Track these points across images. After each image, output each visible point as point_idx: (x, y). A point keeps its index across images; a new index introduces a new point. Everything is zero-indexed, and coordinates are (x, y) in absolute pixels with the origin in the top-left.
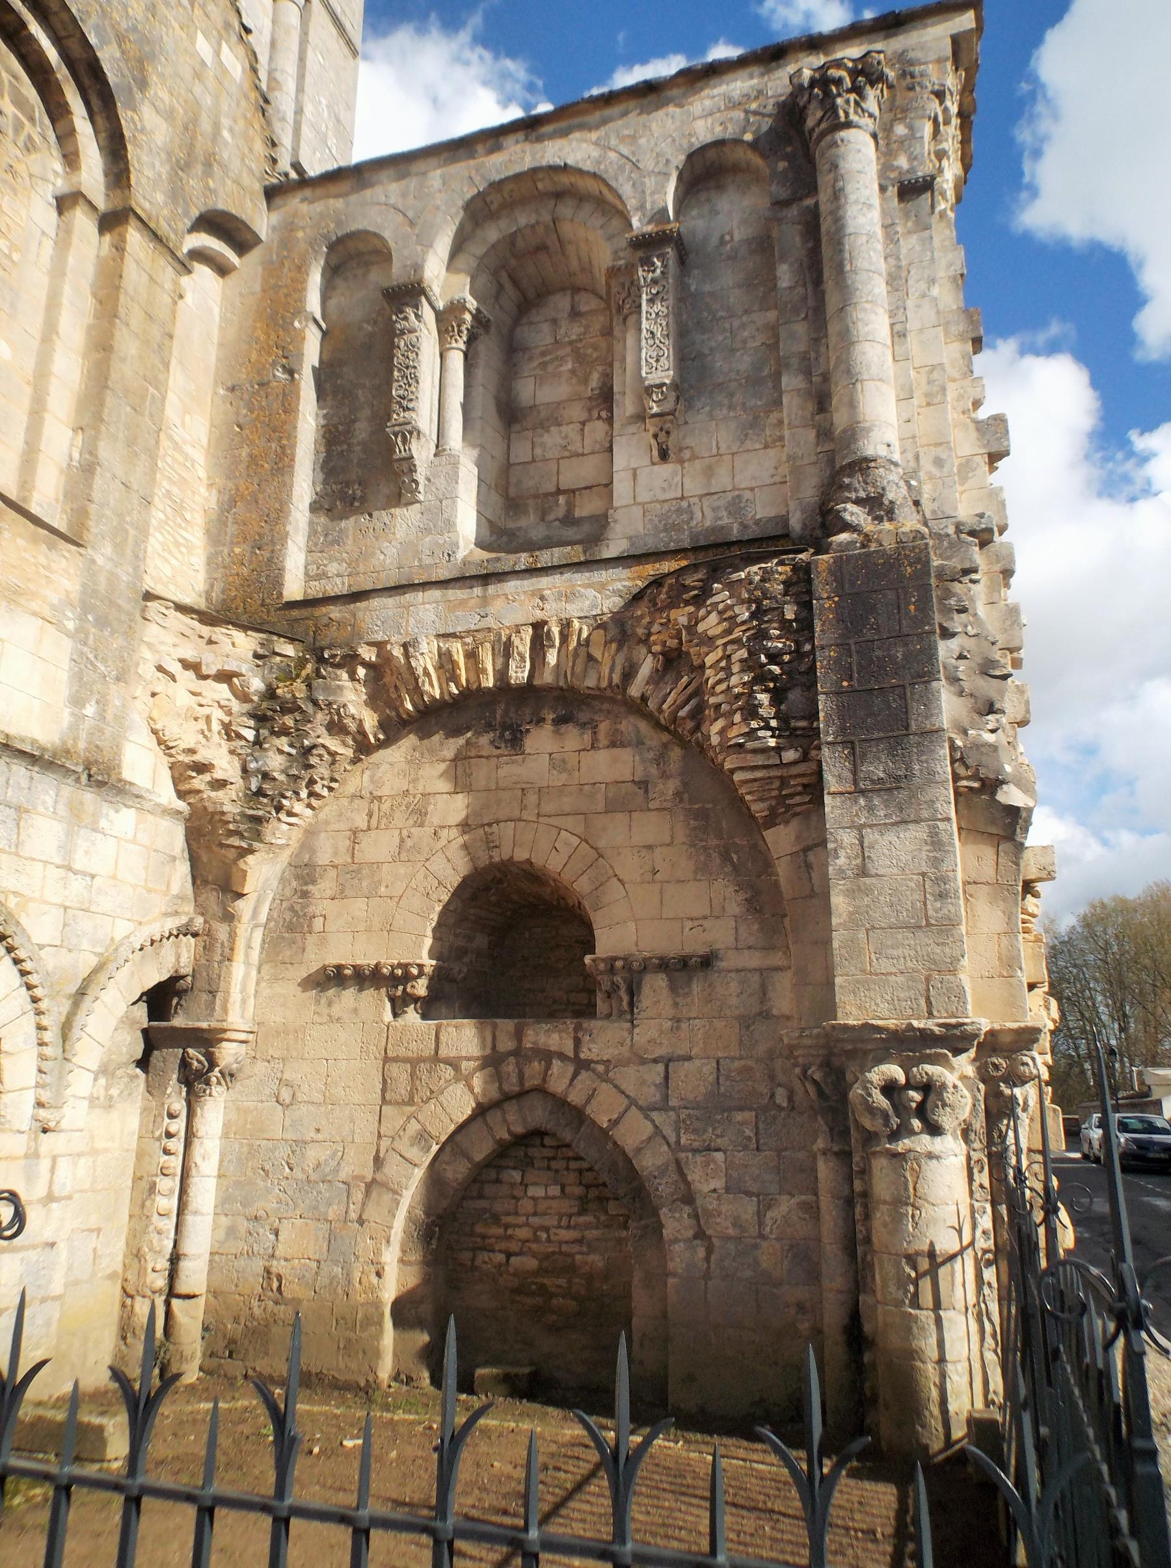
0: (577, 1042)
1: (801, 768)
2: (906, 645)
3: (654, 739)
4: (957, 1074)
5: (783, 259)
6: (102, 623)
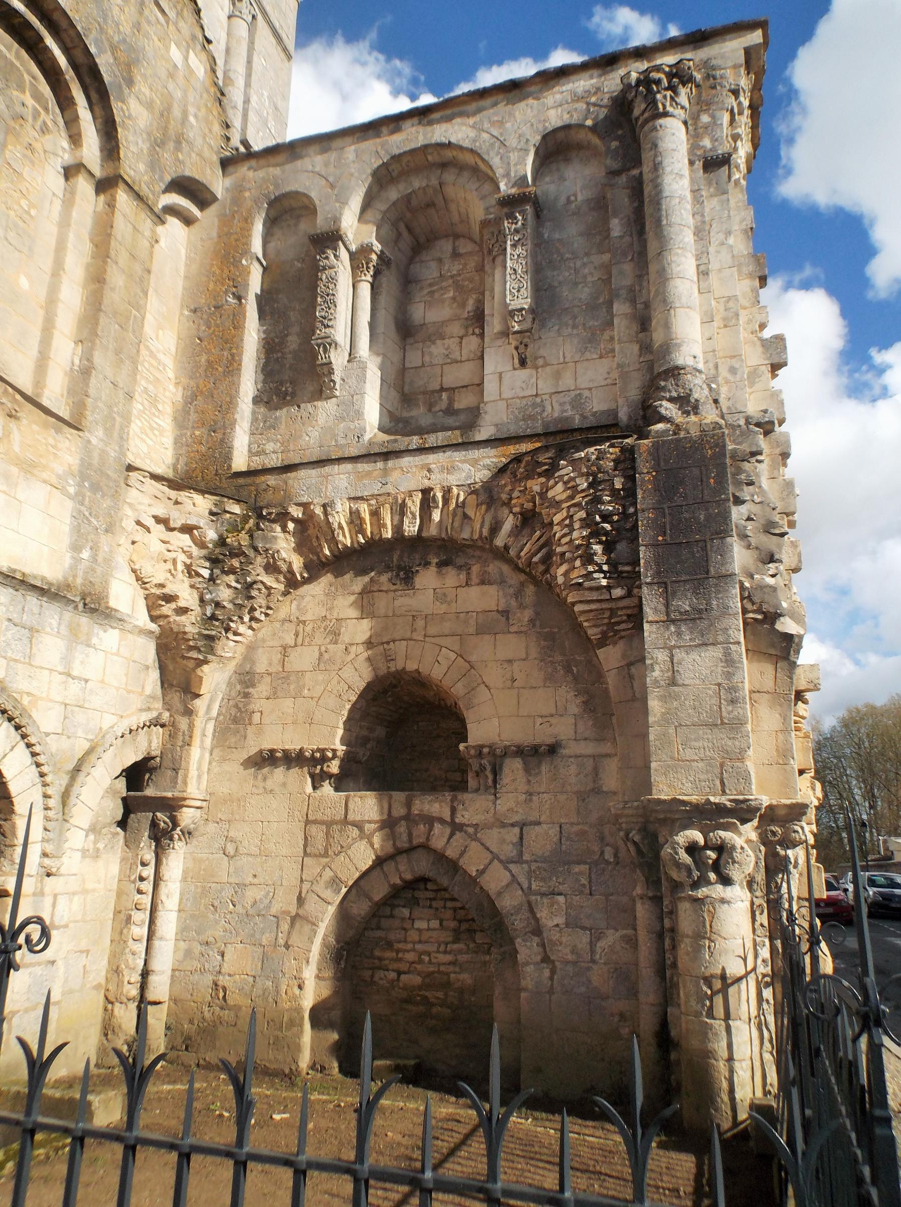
0: (453, 811)
2: (707, 509)
3: (514, 579)
4: (744, 838)
5: (615, 215)
6: (95, 488)
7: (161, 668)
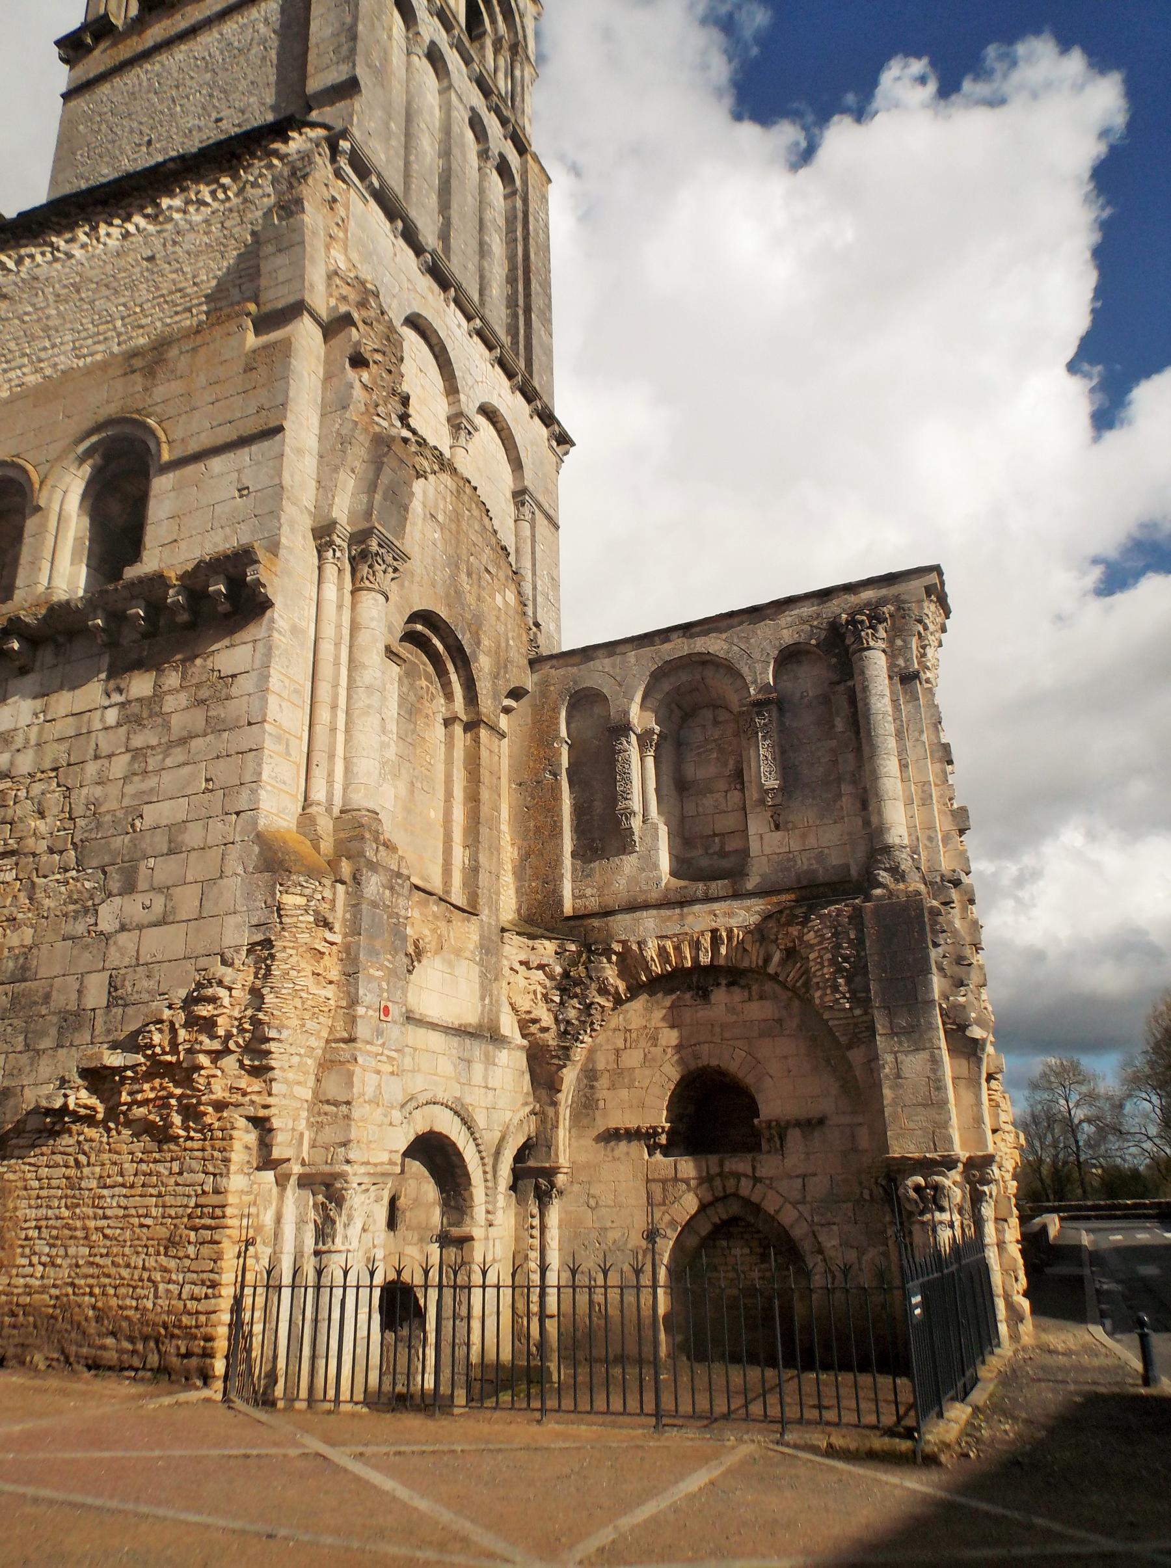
0: (754, 1168)
1: (865, 1018)
3: (784, 995)
4: (952, 1182)
7: (531, 1071)
